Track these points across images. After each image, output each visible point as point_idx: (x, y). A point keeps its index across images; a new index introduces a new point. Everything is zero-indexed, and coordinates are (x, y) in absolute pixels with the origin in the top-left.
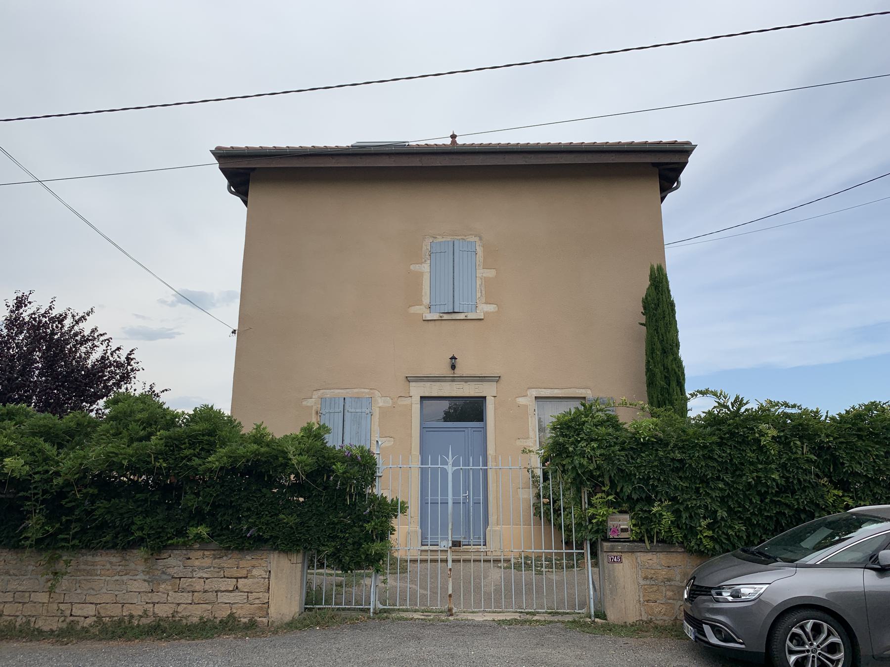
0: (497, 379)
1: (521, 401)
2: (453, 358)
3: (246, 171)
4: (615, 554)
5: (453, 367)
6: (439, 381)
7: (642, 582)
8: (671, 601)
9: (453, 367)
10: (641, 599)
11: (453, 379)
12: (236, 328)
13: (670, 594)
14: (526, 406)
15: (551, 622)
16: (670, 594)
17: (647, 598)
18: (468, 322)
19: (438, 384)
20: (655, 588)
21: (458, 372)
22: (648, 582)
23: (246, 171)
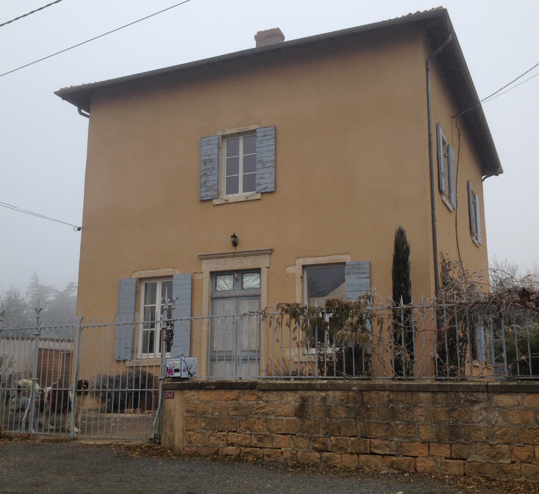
0: (271, 252)
1: (290, 270)
2: (234, 236)
3: (83, 97)
4: (170, 391)
5: (235, 244)
6: (223, 257)
7: (185, 414)
8: (203, 431)
9: (235, 244)
10: (184, 429)
11: (234, 255)
12: (80, 225)
13: (203, 424)
14: (294, 275)
15: (57, 441)
16: (203, 424)
17: (188, 428)
18: (229, 205)
19: (222, 260)
20: (194, 419)
21: (240, 248)
22: (189, 415)
23: (83, 97)
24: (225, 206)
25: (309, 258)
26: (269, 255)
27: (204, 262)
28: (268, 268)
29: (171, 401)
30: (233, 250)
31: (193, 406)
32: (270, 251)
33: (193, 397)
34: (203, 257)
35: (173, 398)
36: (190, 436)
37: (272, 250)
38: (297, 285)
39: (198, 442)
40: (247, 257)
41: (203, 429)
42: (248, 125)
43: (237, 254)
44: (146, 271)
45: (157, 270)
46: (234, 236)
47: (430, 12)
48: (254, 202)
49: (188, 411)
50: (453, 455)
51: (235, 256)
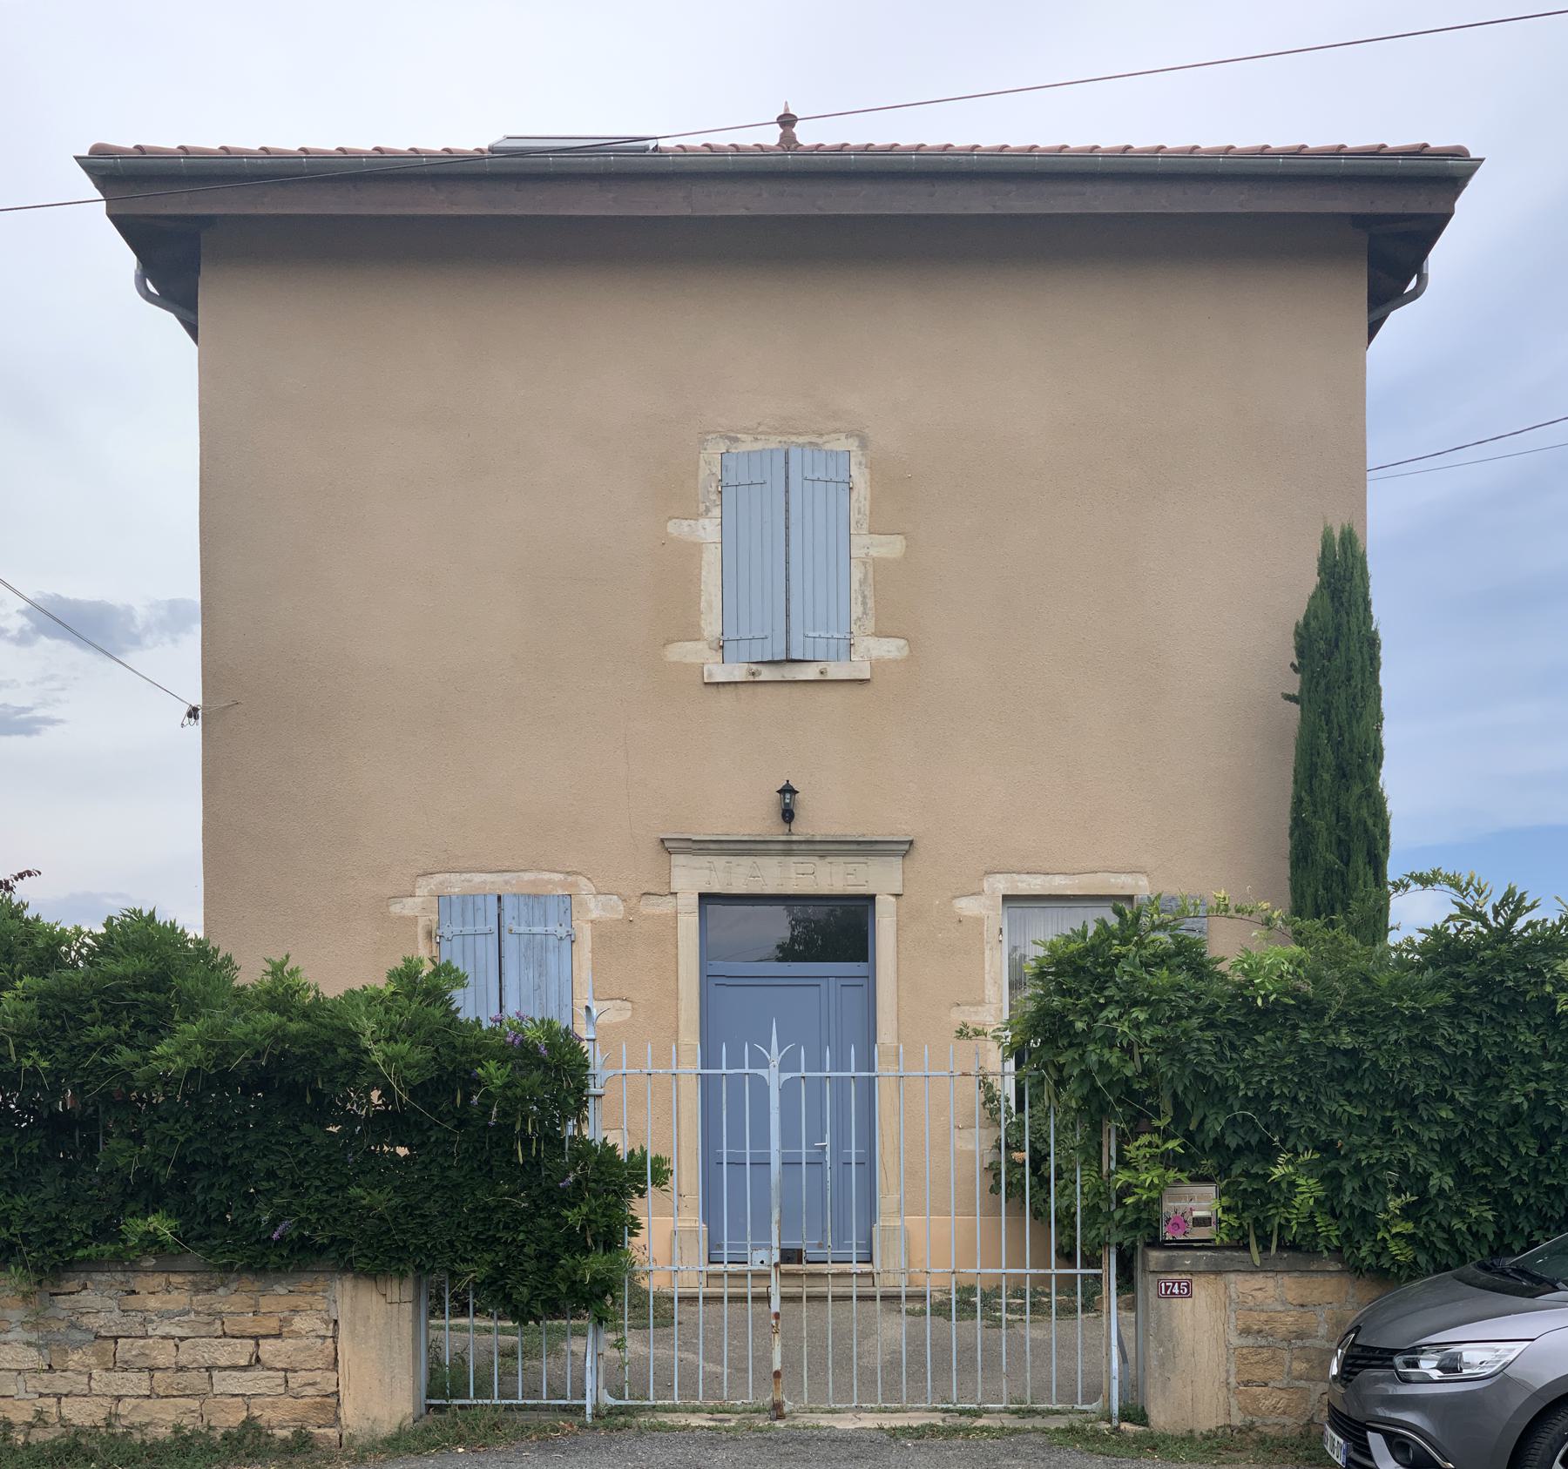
2: (788, 790)
3: (195, 224)
5: (788, 815)
7: (1236, 1341)
8: (1302, 1383)
9: (788, 815)
10: (1232, 1380)
11: (788, 848)
12: (197, 701)
14: (979, 921)
15: (1015, 1431)
17: (1246, 1377)
18: (760, 689)
19: (746, 861)
20: (1266, 1354)
21: (803, 828)
22: (1250, 1341)
24: (745, 692)
25: (1025, 876)
26: (897, 861)
27: (678, 859)
28: (897, 895)
29: (1182, 1306)
30: (776, 831)
31: (1264, 1317)
34: (669, 847)
35: (1189, 1295)
36: (1255, 1399)
37: (911, 843)
38: (987, 952)
40: (829, 859)
41: (1299, 1378)
42: (821, 435)
45: (507, 876)
46: (788, 790)
47: (1215, 153)
50: (110, 1345)
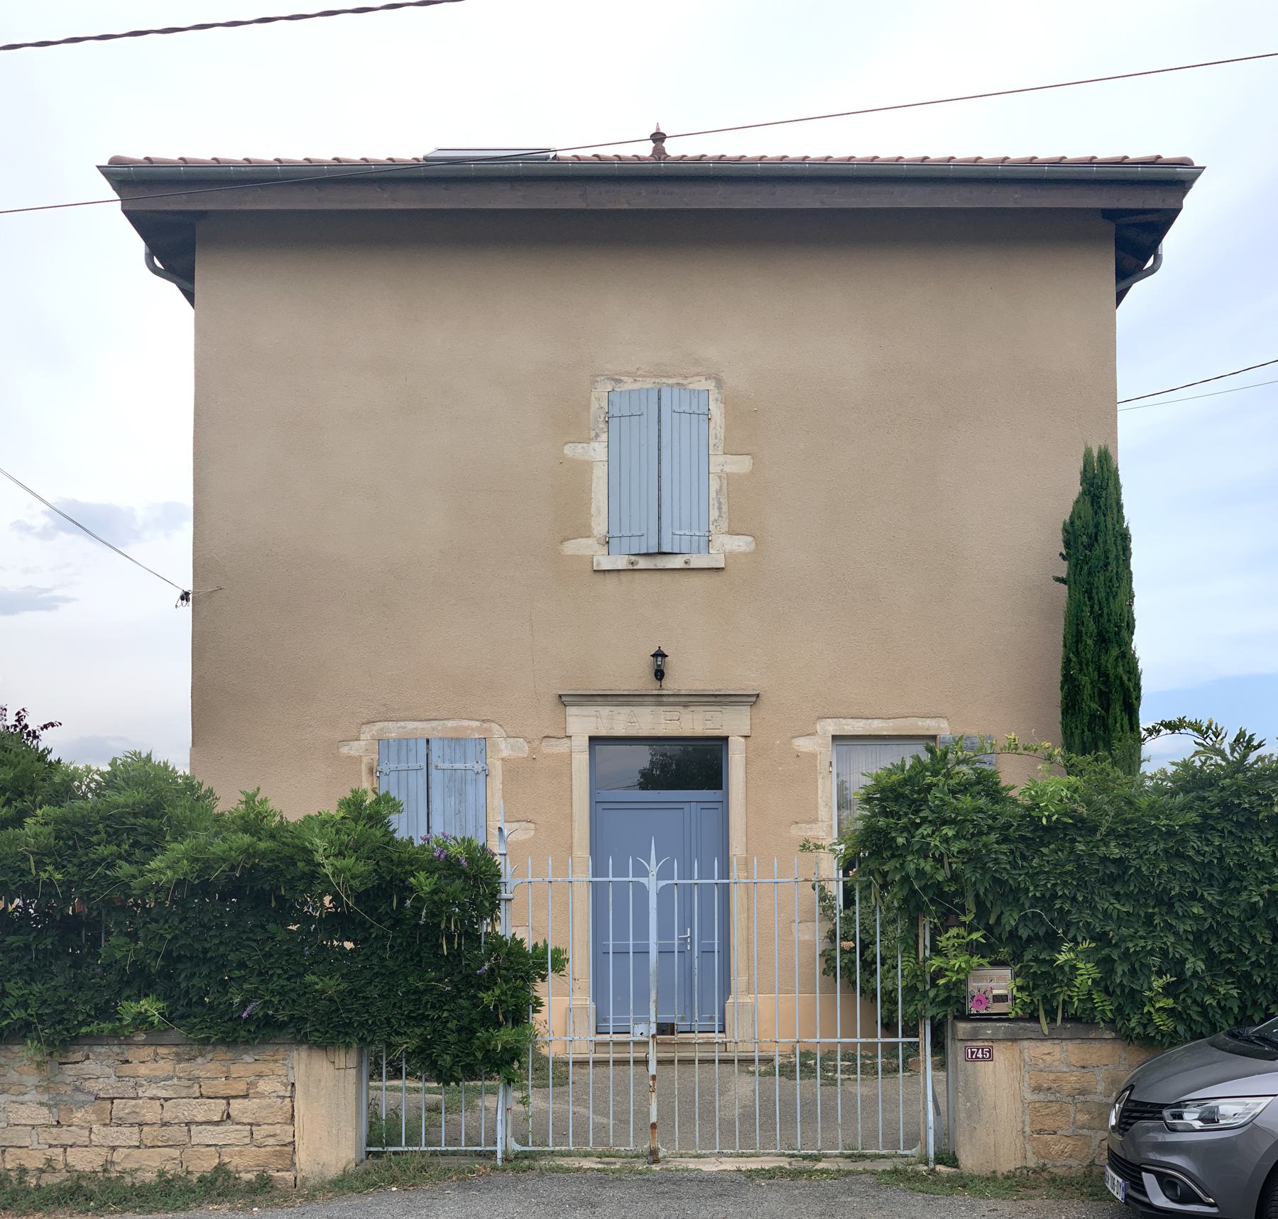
0: (752, 700)
1: (804, 744)
2: (659, 655)
3: (189, 218)
5: (659, 674)
7: (1029, 1097)
8: (1085, 1132)
9: (659, 674)
10: (1027, 1129)
11: (659, 699)
12: (189, 587)
14: (813, 756)
15: (849, 1173)
19: (625, 710)
20: (1055, 1107)
21: (670, 685)
22: (1041, 1097)
23: (189, 218)
27: (572, 710)
31: (1052, 1076)
32: (754, 699)
33: (1047, 1058)
35: (991, 1059)
36: (1046, 1144)
37: (758, 695)
38: (820, 781)
39: (1071, 1156)
40: (692, 708)
41: (1082, 1127)
43: (665, 699)
44: (402, 724)
45: (434, 724)
46: (659, 655)
48: (671, 573)
49: (1037, 1089)
50: (107, 1104)
51: (661, 704)
